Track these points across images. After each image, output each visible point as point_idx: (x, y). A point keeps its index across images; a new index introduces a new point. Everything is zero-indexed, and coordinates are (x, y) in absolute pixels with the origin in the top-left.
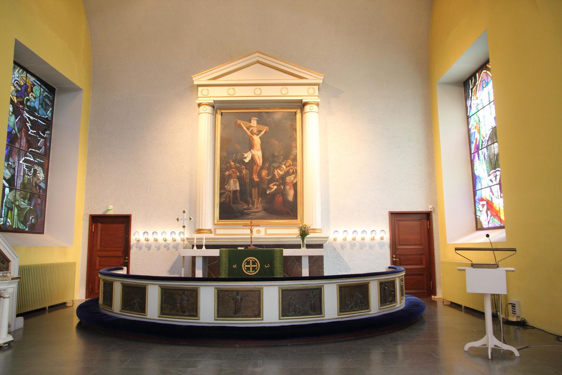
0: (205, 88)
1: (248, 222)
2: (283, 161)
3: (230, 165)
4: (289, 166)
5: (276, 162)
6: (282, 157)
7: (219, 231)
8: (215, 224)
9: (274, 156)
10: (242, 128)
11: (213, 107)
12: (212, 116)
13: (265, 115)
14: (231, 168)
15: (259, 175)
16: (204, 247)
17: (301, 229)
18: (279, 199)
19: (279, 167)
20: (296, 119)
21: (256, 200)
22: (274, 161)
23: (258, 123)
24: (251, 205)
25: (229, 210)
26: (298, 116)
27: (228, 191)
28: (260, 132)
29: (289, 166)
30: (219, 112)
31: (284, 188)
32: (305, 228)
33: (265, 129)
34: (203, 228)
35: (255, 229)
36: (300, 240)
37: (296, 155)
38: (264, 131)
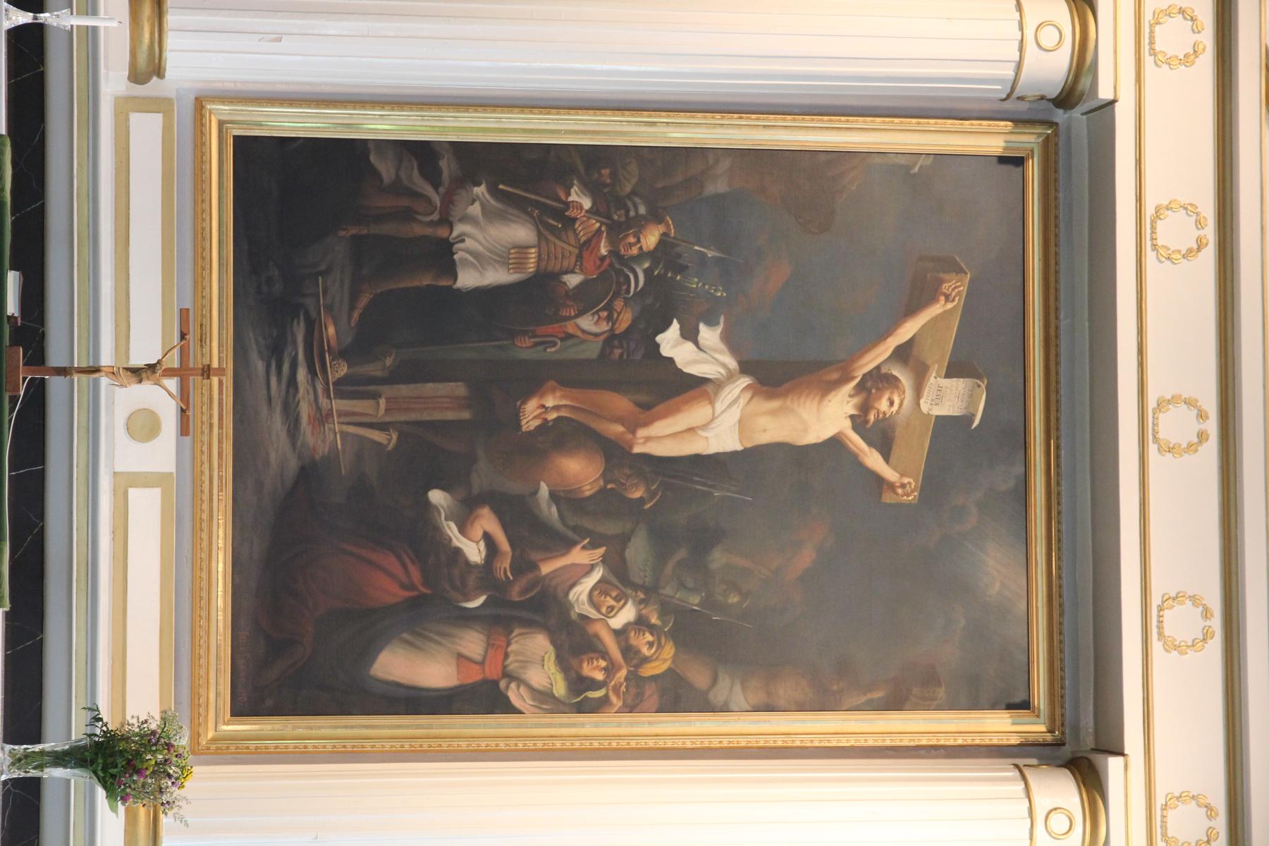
0: (1207, 38)
1: (217, 348)
2: (666, 609)
3: (638, 225)
4: (629, 651)
5: (661, 552)
6: (694, 600)
7: (147, 131)
8: (199, 104)
9: (703, 539)
10: (911, 310)
11: (1067, 98)
12: (1001, 90)
13: (1004, 479)
14: (616, 230)
15: (563, 435)
16: (23, 18)
17: (152, 740)
18: (388, 580)
19: (620, 579)
20: (974, 705)
21: (379, 409)
22: (663, 540)
23: (948, 429)
24: (343, 370)
25: (317, 216)
26: (999, 725)
27: (448, 201)
28: (883, 438)
29: (629, 651)
30: (1029, 140)
31: (468, 619)
32: (161, 771)
33: (899, 475)
34: (171, 19)
35: (160, 398)
36: (78, 732)
37: (704, 705)
38: (889, 473)
